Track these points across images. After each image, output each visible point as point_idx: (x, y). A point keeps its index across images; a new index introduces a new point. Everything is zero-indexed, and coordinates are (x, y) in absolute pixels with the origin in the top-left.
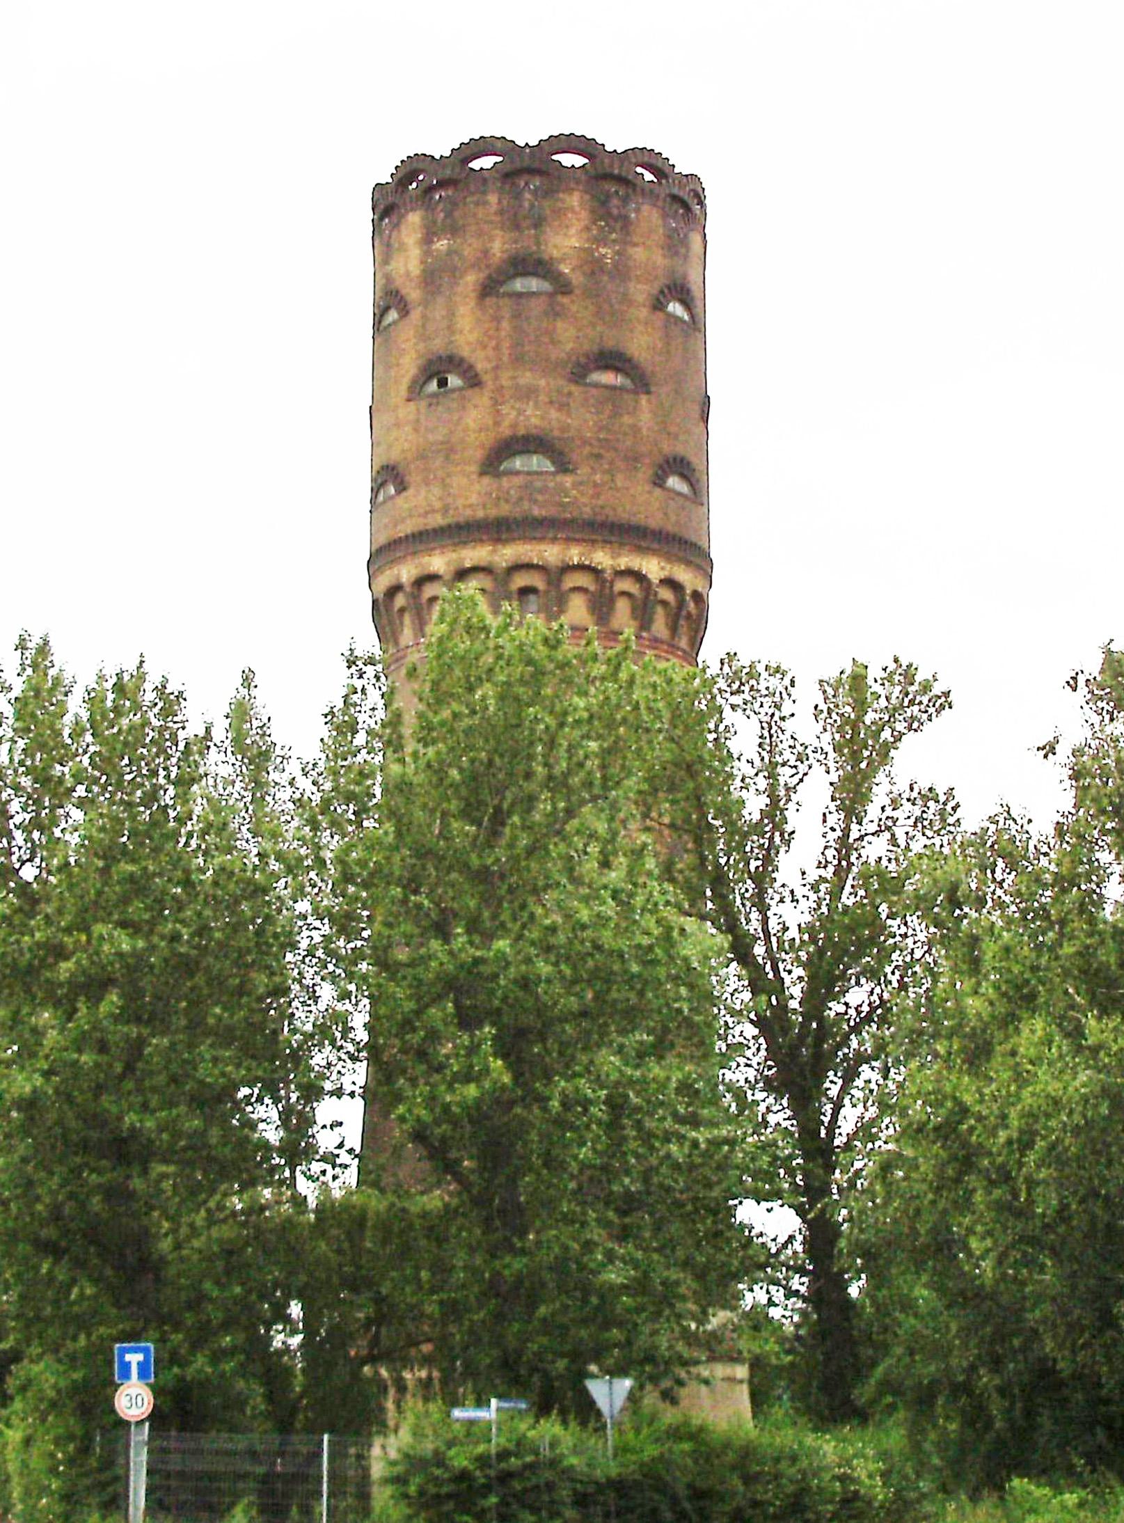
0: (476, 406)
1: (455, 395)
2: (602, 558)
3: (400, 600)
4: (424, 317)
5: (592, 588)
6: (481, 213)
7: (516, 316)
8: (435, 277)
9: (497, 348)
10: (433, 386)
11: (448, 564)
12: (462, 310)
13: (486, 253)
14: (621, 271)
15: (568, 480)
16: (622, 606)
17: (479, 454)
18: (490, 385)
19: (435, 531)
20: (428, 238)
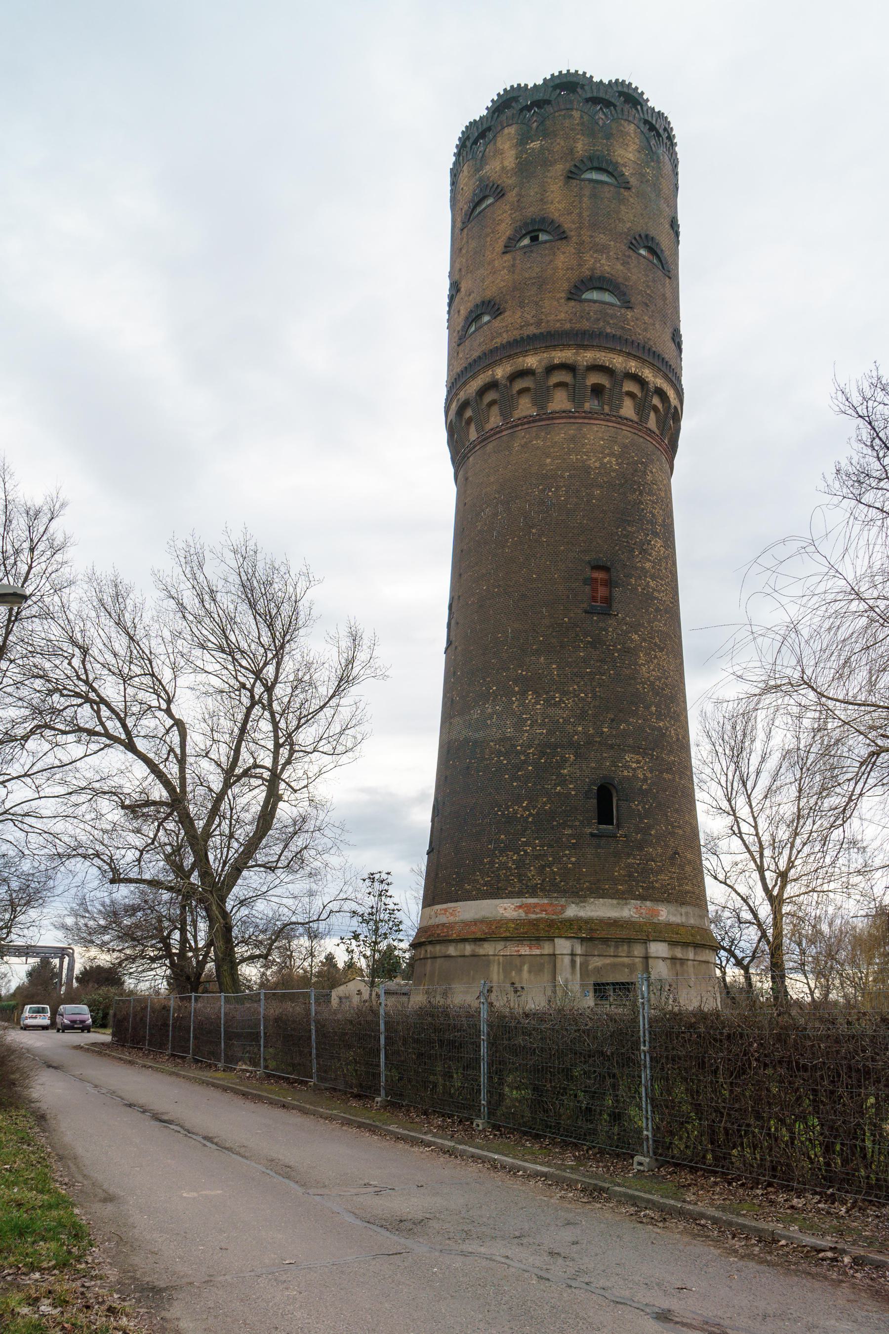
0: (564, 253)
4: (519, 195)
6: (567, 123)
7: (594, 196)
9: (580, 215)
10: (526, 241)
11: (540, 362)
12: (554, 188)
13: (571, 151)
15: (629, 314)
17: (566, 286)
18: (574, 239)
20: (523, 140)
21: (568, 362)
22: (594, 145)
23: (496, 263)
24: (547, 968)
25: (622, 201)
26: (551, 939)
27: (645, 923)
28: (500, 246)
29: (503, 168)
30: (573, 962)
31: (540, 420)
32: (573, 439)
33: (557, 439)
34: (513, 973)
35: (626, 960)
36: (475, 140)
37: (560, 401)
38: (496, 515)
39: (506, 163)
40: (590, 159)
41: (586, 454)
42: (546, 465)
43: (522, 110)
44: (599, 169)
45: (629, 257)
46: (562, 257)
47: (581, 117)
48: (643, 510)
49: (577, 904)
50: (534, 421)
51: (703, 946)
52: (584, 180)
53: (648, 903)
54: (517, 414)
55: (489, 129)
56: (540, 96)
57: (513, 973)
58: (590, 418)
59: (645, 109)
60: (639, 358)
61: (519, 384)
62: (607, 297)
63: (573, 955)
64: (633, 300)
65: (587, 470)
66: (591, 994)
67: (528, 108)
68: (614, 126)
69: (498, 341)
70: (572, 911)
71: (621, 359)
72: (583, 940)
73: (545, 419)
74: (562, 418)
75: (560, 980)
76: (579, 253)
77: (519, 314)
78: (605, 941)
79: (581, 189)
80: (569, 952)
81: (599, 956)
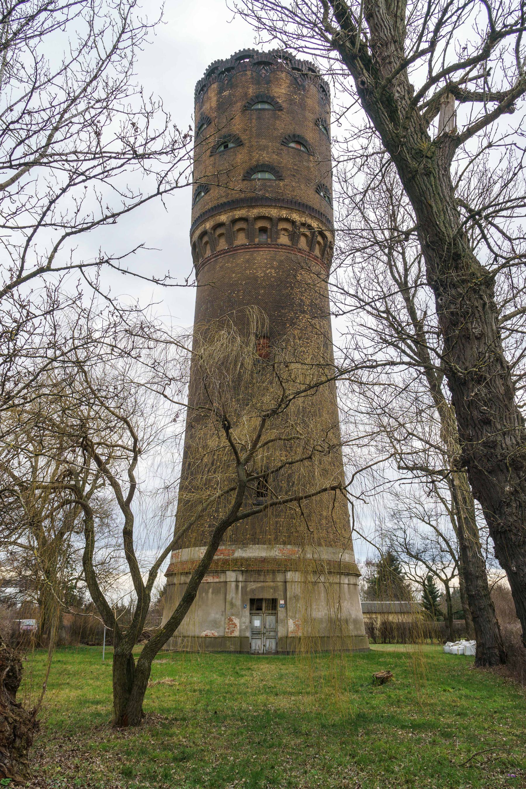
1: (232, 150)
2: (295, 217)
3: (206, 239)
5: (291, 229)
6: (243, 79)
7: (259, 118)
8: (223, 106)
10: (222, 148)
11: (228, 218)
13: (246, 94)
14: (303, 106)
15: (282, 184)
16: (303, 240)
18: (247, 145)
19: (161, 564)
20: (220, 91)
21: (243, 216)
22: (259, 89)
23: (207, 162)
24: (223, 590)
25: (277, 118)
26: (224, 572)
27: (286, 560)
28: (208, 153)
29: (211, 107)
30: (237, 587)
31: (229, 252)
32: (248, 261)
33: (239, 262)
34: (204, 594)
35: (272, 584)
36: (202, 88)
37: (241, 239)
38: (207, 309)
39: (212, 105)
40: (257, 97)
41: (255, 269)
42: (233, 278)
43: (219, 74)
44: (263, 102)
45: (282, 150)
46: (240, 156)
47: (252, 74)
48: (293, 298)
49: (241, 549)
50: (226, 252)
51: (351, 574)
52: (253, 110)
53: (289, 547)
54: (219, 248)
55: (205, 86)
56: (229, 65)
57: (204, 594)
58: (258, 248)
59: (293, 62)
60: (289, 208)
61: (219, 231)
62: (267, 176)
63: (237, 581)
64: (284, 174)
65: (256, 278)
66: (248, 607)
67: (222, 73)
68: (272, 75)
69: (208, 207)
70: (239, 553)
71: (276, 211)
72: (242, 571)
73: (233, 250)
74: (242, 249)
75: (229, 598)
76: (250, 152)
77: (217, 191)
78: (259, 572)
79: (251, 115)
80: (235, 580)
81: (254, 582)
